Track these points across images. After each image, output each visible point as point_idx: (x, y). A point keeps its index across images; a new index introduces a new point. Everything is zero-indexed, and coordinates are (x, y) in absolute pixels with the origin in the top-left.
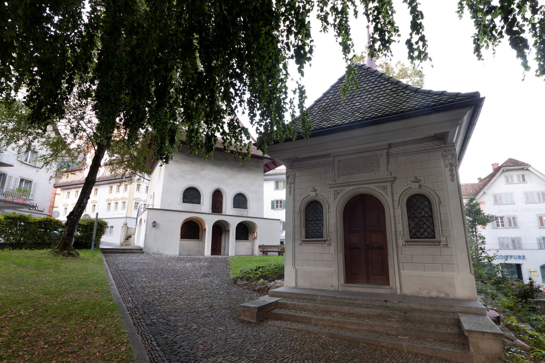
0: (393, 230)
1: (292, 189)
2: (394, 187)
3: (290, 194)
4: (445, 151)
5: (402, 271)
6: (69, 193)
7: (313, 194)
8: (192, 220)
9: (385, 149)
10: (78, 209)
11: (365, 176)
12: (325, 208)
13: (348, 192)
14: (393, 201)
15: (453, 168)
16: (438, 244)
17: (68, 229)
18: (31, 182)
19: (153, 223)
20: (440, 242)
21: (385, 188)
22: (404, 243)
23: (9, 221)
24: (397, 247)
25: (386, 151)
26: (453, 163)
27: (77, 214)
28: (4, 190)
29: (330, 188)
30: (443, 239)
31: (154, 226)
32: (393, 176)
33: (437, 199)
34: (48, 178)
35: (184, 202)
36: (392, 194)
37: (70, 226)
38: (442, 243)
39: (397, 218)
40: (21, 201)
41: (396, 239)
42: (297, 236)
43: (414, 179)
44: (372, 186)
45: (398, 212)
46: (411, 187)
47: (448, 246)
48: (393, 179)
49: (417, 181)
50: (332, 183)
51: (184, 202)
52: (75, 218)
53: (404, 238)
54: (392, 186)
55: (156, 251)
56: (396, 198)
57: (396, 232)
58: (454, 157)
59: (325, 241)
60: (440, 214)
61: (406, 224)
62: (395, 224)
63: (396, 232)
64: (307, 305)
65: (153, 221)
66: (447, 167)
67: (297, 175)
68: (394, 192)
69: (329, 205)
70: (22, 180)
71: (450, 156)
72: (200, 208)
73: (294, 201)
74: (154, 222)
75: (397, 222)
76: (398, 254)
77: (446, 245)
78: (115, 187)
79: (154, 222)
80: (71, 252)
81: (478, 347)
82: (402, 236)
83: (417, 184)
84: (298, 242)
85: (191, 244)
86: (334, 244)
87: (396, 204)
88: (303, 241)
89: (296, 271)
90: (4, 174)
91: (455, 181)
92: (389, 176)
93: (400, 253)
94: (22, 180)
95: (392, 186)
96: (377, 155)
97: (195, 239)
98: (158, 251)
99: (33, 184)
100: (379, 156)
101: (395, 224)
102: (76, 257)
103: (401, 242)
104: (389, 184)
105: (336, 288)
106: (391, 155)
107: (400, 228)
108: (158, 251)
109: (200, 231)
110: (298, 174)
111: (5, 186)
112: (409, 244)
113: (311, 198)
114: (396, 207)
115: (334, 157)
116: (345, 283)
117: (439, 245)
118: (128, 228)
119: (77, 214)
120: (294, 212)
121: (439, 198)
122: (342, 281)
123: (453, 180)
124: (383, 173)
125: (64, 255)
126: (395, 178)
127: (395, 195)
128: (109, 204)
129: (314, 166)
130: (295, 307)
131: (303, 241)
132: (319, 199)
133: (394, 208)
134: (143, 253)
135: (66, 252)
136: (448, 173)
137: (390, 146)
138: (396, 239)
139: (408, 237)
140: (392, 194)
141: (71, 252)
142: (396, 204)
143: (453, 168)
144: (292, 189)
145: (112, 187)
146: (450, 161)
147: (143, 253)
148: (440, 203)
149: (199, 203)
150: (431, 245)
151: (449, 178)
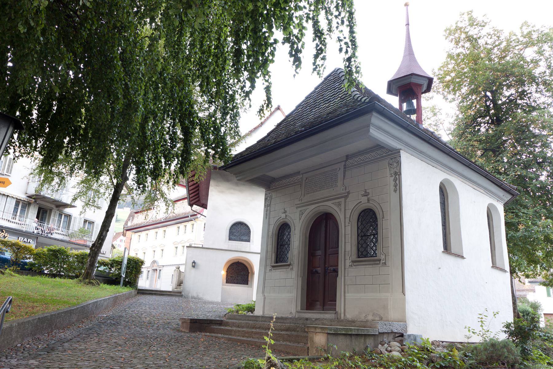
0: (343, 250)
1: (268, 212)
2: (347, 203)
3: (266, 218)
4: (391, 159)
5: (347, 294)
6: (140, 236)
7: (283, 216)
8: (240, 261)
9: (343, 161)
10: (98, 241)
11: (325, 193)
12: (292, 229)
13: (311, 210)
14: (345, 218)
15: (397, 177)
16: (378, 262)
17: (90, 260)
18: (93, 222)
19: (193, 263)
20: (380, 260)
21: (339, 204)
22: (351, 264)
23: (51, 253)
24: (345, 269)
25: (343, 163)
26: (397, 171)
27: (98, 246)
28: (70, 231)
29: (297, 208)
30: (383, 257)
31: (194, 267)
32: (347, 190)
33: (381, 213)
34: (79, 213)
35: (230, 239)
36: (345, 210)
37: (92, 257)
38: (382, 262)
39: (347, 236)
40: (82, 242)
41: (345, 260)
42: (269, 262)
43: (363, 193)
44: (329, 203)
45: (349, 229)
46: (361, 202)
47: (386, 265)
48: (347, 194)
49: (366, 194)
50: (299, 202)
51: (230, 239)
52: (96, 250)
53: (351, 258)
54: (345, 202)
55: (195, 295)
56: (348, 216)
57: (345, 251)
58: (398, 165)
59: (289, 265)
60: (382, 229)
61: (355, 242)
62: (345, 243)
63: (345, 251)
64: (241, 323)
65: (192, 261)
66: (392, 176)
67: (273, 197)
68: (347, 208)
69: (295, 226)
70: (85, 221)
71: (395, 164)
72: (250, 247)
73: (269, 225)
74: (194, 262)
75: (347, 241)
76: (345, 276)
77: (385, 263)
78: (182, 226)
79: (194, 262)
80: (92, 281)
81: (313, 341)
82: (349, 256)
83: (366, 198)
84: (269, 268)
85: (237, 290)
86: (295, 268)
87: (347, 220)
88: (273, 267)
89: (265, 298)
90: (70, 215)
91: (398, 191)
92: (344, 191)
93: (346, 275)
94: (85, 221)
95: (345, 202)
96: (336, 169)
97: (244, 284)
98: (198, 296)
99: (95, 224)
100: (338, 169)
101: (345, 243)
102: (95, 286)
103: (348, 263)
104: (343, 200)
105: (294, 315)
106: (348, 167)
107: (348, 248)
108: (198, 296)
109: (250, 274)
110: (274, 195)
111: (71, 228)
112: (355, 264)
113: (282, 221)
114: (347, 225)
115: (302, 174)
116: (301, 309)
117: (379, 264)
118: (180, 272)
119: (98, 246)
120: (268, 236)
121: (383, 212)
122: (299, 308)
123: (395, 191)
124: (339, 189)
125: (85, 283)
126: (349, 193)
127: (347, 211)
128: (177, 248)
129: (286, 185)
130: (233, 325)
131: (273, 267)
132: (289, 221)
133: (345, 226)
134: (182, 296)
135: (87, 280)
136: (392, 183)
137: (348, 157)
138: (345, 260)
139: (354, 257)
140: (345, 210)
141: (92, 281)
142: (347, 220)
143: (397, 177)
144: (268, 212)
145: (179, 227)
146: (395, 169)
147: (182, 296)
148: (383, 218)
149: (248, 241)
150: (372, 264)
151: (392, 188)
